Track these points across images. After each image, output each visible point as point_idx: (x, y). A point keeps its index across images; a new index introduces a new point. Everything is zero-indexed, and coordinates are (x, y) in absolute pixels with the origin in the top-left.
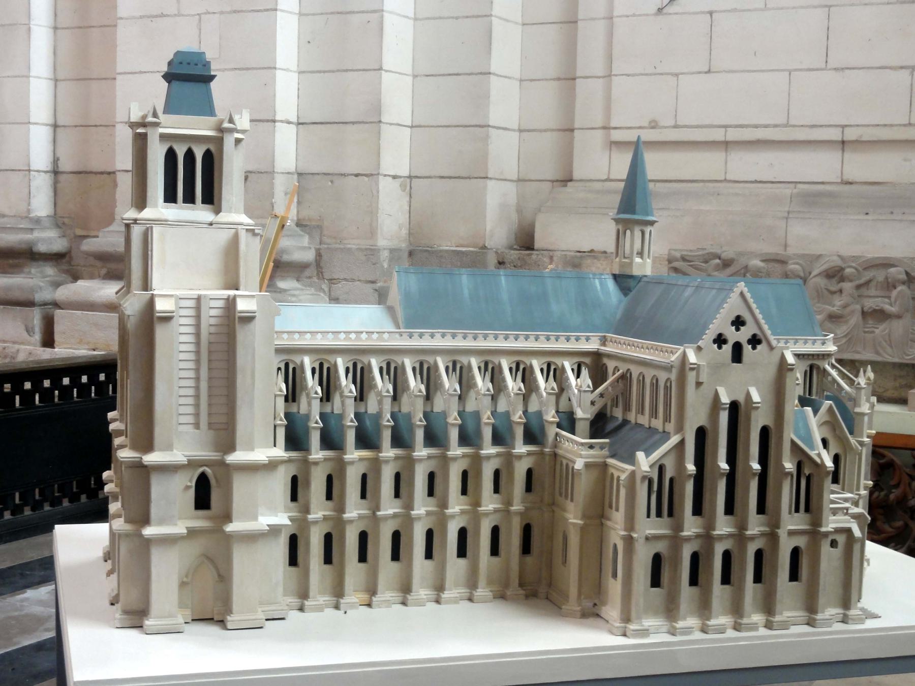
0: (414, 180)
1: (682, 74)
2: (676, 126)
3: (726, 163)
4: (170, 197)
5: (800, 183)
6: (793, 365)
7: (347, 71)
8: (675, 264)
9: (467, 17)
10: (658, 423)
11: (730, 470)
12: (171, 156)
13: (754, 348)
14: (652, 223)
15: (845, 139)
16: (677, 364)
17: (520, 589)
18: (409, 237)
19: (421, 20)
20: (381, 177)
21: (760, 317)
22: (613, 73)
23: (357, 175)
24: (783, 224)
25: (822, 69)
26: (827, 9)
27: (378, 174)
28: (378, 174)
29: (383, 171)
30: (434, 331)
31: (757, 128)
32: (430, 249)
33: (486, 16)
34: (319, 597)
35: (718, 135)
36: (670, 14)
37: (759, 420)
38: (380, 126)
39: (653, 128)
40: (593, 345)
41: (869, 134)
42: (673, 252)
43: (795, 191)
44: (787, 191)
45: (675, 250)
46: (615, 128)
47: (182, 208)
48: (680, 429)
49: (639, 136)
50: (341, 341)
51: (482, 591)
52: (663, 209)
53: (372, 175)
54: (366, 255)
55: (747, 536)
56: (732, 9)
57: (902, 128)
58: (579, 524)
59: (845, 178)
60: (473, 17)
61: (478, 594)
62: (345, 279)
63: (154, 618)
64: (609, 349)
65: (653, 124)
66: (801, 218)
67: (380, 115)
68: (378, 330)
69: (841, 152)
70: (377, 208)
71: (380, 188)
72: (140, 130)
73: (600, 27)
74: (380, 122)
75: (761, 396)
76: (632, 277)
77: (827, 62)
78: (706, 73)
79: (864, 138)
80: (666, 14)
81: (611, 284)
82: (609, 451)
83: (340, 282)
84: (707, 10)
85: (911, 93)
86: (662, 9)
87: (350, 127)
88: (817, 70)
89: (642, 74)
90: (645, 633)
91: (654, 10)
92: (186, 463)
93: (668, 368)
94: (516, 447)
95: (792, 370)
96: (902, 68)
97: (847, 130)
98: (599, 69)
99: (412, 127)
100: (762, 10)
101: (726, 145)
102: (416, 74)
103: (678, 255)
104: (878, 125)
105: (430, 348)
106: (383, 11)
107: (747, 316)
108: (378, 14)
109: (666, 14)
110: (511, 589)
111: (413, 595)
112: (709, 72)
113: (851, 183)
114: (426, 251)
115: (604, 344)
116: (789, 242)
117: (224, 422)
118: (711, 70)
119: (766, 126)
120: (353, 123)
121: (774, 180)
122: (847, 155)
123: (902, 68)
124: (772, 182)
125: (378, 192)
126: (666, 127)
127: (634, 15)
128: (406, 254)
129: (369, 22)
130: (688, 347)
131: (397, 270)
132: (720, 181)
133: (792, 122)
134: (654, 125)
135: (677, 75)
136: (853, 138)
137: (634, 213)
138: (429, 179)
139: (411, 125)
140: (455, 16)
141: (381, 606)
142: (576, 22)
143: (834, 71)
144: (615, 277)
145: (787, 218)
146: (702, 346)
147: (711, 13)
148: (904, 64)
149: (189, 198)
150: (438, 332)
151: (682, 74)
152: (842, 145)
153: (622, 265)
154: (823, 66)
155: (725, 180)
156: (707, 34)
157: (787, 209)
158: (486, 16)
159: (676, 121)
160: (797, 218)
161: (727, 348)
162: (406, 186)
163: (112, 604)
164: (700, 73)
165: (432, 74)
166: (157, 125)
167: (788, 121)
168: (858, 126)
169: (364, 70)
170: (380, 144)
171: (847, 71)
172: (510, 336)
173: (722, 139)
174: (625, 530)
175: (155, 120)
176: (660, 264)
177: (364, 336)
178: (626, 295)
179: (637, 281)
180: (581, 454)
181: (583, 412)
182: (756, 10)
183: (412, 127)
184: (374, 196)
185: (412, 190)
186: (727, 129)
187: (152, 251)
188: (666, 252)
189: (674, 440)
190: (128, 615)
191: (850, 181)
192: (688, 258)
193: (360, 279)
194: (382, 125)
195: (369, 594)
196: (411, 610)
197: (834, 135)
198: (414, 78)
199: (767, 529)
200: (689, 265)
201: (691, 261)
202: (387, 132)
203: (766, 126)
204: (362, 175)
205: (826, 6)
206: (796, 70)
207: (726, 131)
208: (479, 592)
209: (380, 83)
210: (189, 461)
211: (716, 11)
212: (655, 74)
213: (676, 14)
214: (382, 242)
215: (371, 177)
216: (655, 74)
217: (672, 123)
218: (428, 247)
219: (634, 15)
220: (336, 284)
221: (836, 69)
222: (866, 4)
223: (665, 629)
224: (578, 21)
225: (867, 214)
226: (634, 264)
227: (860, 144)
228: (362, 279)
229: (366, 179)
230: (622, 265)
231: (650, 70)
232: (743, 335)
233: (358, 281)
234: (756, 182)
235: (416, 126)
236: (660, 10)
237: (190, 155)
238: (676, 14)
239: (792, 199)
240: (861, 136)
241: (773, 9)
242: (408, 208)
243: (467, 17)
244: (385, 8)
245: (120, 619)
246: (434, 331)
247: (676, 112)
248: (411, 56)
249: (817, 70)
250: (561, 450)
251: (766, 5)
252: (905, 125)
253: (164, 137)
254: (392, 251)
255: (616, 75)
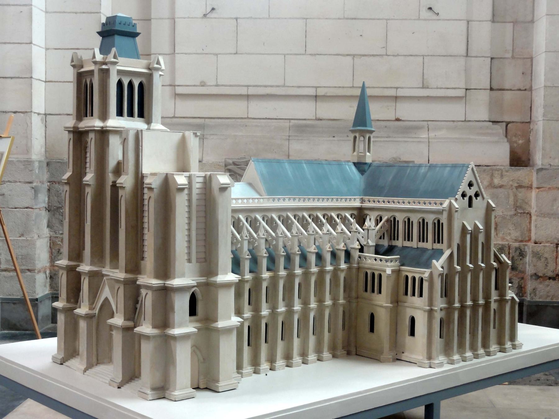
0: (48, 116)
1: (220, 54)
2: (217, 85)
3: (248, 107)
4: (120, 113)
5: (292, 119)
6: (494, 208)
7: (5, 43)
8: (229, 167)
9: (84, 13)
10: (429, 245)
11: (474, 267)
12: (120, 84)
13: (476, 199)
14: (371, 132)
15: (318, 94)
16: (447, 209)
17: (343, 350)
18: (46, 153)
19: (50, 13)
20: (33, 114)
21: (479, 181)
22: (176, 52)
23: (15, 112)
24: (287, 143)
25: (303, 54)
26: (305, 20)
27: (31, 112)
28: (31, 112)
29: (34, 110)
30: (285, 197)
31: (266, 87)
32: (61, 161)
33: (97, 13)
34: (248, 369)
35: (244, 91)
36: (211, 18)
37: (481, 238)
38: (32, 80)
39: (202, 86)
40: (357, 204)
41: (331, 92)
42: (228, 160)
43: (291, 124)
44: (287, 124)
45: (229, 159)
46: (179, 86)
47: (127, 120)
48: (449, 246)
49: (364, 82)
50: (240, 204)
51: (326, 354)
52: (213, 134)
53: (26, 112)
54: (24, 165)
55: (480, 304)
56: (249, 17)
57: (349, 89)
58: (391, 306)
59: (318, 116)
60: (88, 13)
61: (324, 356)
62: (9, 181)
63: (178, 390)
64: (367, 205)
65: (203, 84)
66: (297, 140)
67: (32, 73)
68: (252, 197)
69: (315, 101)
70: (31, 134)
71: (33, 121)
72: (104, 67)
73: (166, 24)
74: (31, 77)
75: (483, 227)
76: (366, 164)
77: (306, 50)
78: (235, 54)
79: (328, 94)
80: (209, 18)
81: (354, 168)
82: (400, 262)
83: (5, 183)
84: (235, 17)
85: (353, 69)
86: (206, 15)
87: (9, 80)
88: (300, 54)
89: (195, 54)
90: (441, 365)
91: (202, 15)
92: (196, 284)
93: (441, 212)
94: (341, 265)
95: (494, 210)
96: (348, 55)
97: (319, 90)
98: (167, 49)
99: (46, 82)
100: (267, 18)
101: (248, 97)
102: (47, 47)
103: (231, 161)
104: (336, 87)
105: (258, 208)
106: (31, 5)
107: (474, 182)
108: (28, 7)
109: (209, 18)
110: (339, 351)
111: (295, 360)
112: (236, 53)
113: (321, 120)
114: (59, 162)
115: (362, 203)
116: (291, 153)
117: (203, 257)
118: (238, 52)
119: (272, 86)
120: (12, 78)
121: (277, 118)
122: (319, 104)
123: (348, 55)
124: (276, 119)
125: (31, 124)
126: (211, 86)
127: (189, 18)
128: (45, 165)
129: (21, 12)
130: (452, 199)
131: (253, 160)
132: (245, 118)
133: (287, 84)
134: (203, 84)
135: (216, 55)
136: (323, 94)
137: (366, 126)
138: (60, 116)
139: (45, 80)
140: (75, 11)
141: (280, 369)
142: (150, 20)
143: (310, 56)
144: (355, 164)
145: (289, 140)
146: (458, 198)
147: (236, 19)
148: (349, 53)
149: (131, 114)
150: (287, 198)
151: (220, 54)
152: (315, 98)
153: (359, 157)
154: (304, 52)
155: (248, 118)
156: (235, 31)
157: (288, 135)
158: (97, 13)
159: (217, 82)
160: (295, 139)
161: (467, 199)
162: (43, 121)
163: (119, 388)
164: (231, 54)
165: (60, 48)
166: (115, 63)
167: (284, 83)
168: (324, 87)
169: (19, 43)
170: (32, 92)
171: (317, 56)
172: (325, 199)
173: (246, 93)
174: (428, 306)
175: (115, 60)
176: (215, 168)
177: (245, 201)
178: (362, 174)
179: (368, 166)
180: (388, 265)
181: (372, 242)
182: (263, 18)
183: (46, 82)
184: (28, 127)
185: (47, 123)
186: (249, 87)
187: (142, 146)
188: (223, 161)
189: (447, 253)
190: (154, 391)
191: (321, 118)
192: (237, 163)
193: (20, 181)
194: (32, 79)
195: (270, 363)
196: (309, 366)
197: (312, 92)
198: (46, 50)
199: (498, 298)
200: (238, 168)
201: (239, 165)
202: (35, 83)
203: (272, 86)
204: (19, 112)
205: (304, 18)
206: (288, 54)
207: (248, 89)
208: (325, 354)
209: (31, 53)
210: (197, 283)
211: (239, 18)
212: (203, 54)
213: (215, 18)
214: (34, 157)
215: (26, 114)
216: (203, 54)
217: (215, 83)
218: (60, 160)
219: (189, 18)
220: (2, 184)
221: (310, 54)
222: (327, 19)
223: (445, 362)
224: (152, 20)
225: (334, 137)
226: (366, 156)
227: (326, 98)
228: (22, 181)
229: (22, 115)
230: (359, 157)
231: (200, 51)
232: (471, 192)
233: (19, 182)
234: (266, 119)
235: (49, 82)
236: (205, 15)
237: (131, 84)
238: (215, 18)
239: (290, 129)
240: (326, 93)
241: (273, 18)
242: (45, 135)
243: (84, 13)
244: (33, 4)
245: (152, 394)
246: (285, 197)
247: (217, 77)
248: (44, 36)
249: (300, 54)
250: (362, 264)
251: (269, 16)
252: (351, 87)
253: (120, 72)
254: (40, 162)
255: (178, 54)
